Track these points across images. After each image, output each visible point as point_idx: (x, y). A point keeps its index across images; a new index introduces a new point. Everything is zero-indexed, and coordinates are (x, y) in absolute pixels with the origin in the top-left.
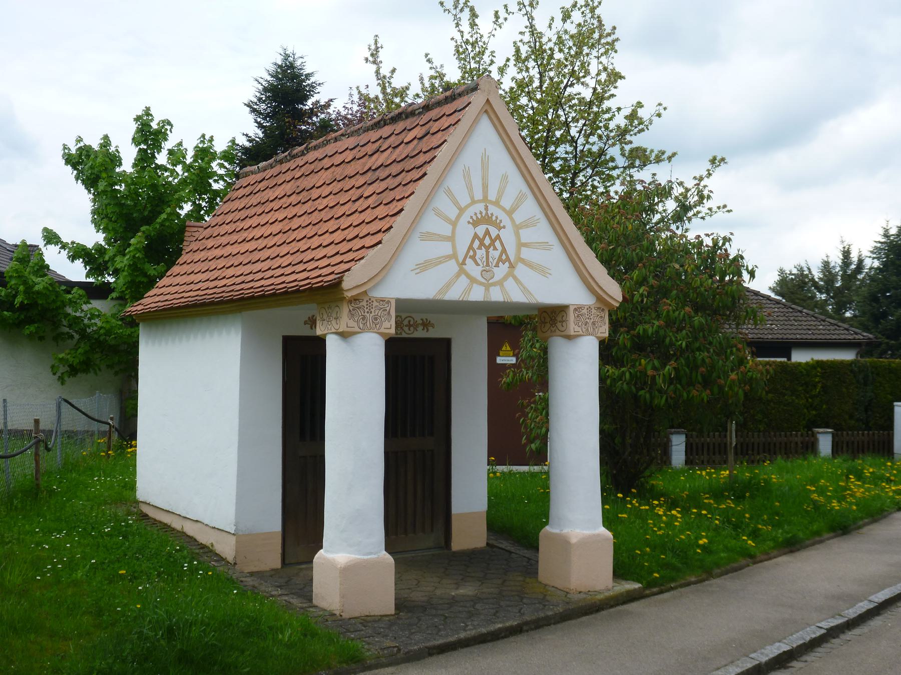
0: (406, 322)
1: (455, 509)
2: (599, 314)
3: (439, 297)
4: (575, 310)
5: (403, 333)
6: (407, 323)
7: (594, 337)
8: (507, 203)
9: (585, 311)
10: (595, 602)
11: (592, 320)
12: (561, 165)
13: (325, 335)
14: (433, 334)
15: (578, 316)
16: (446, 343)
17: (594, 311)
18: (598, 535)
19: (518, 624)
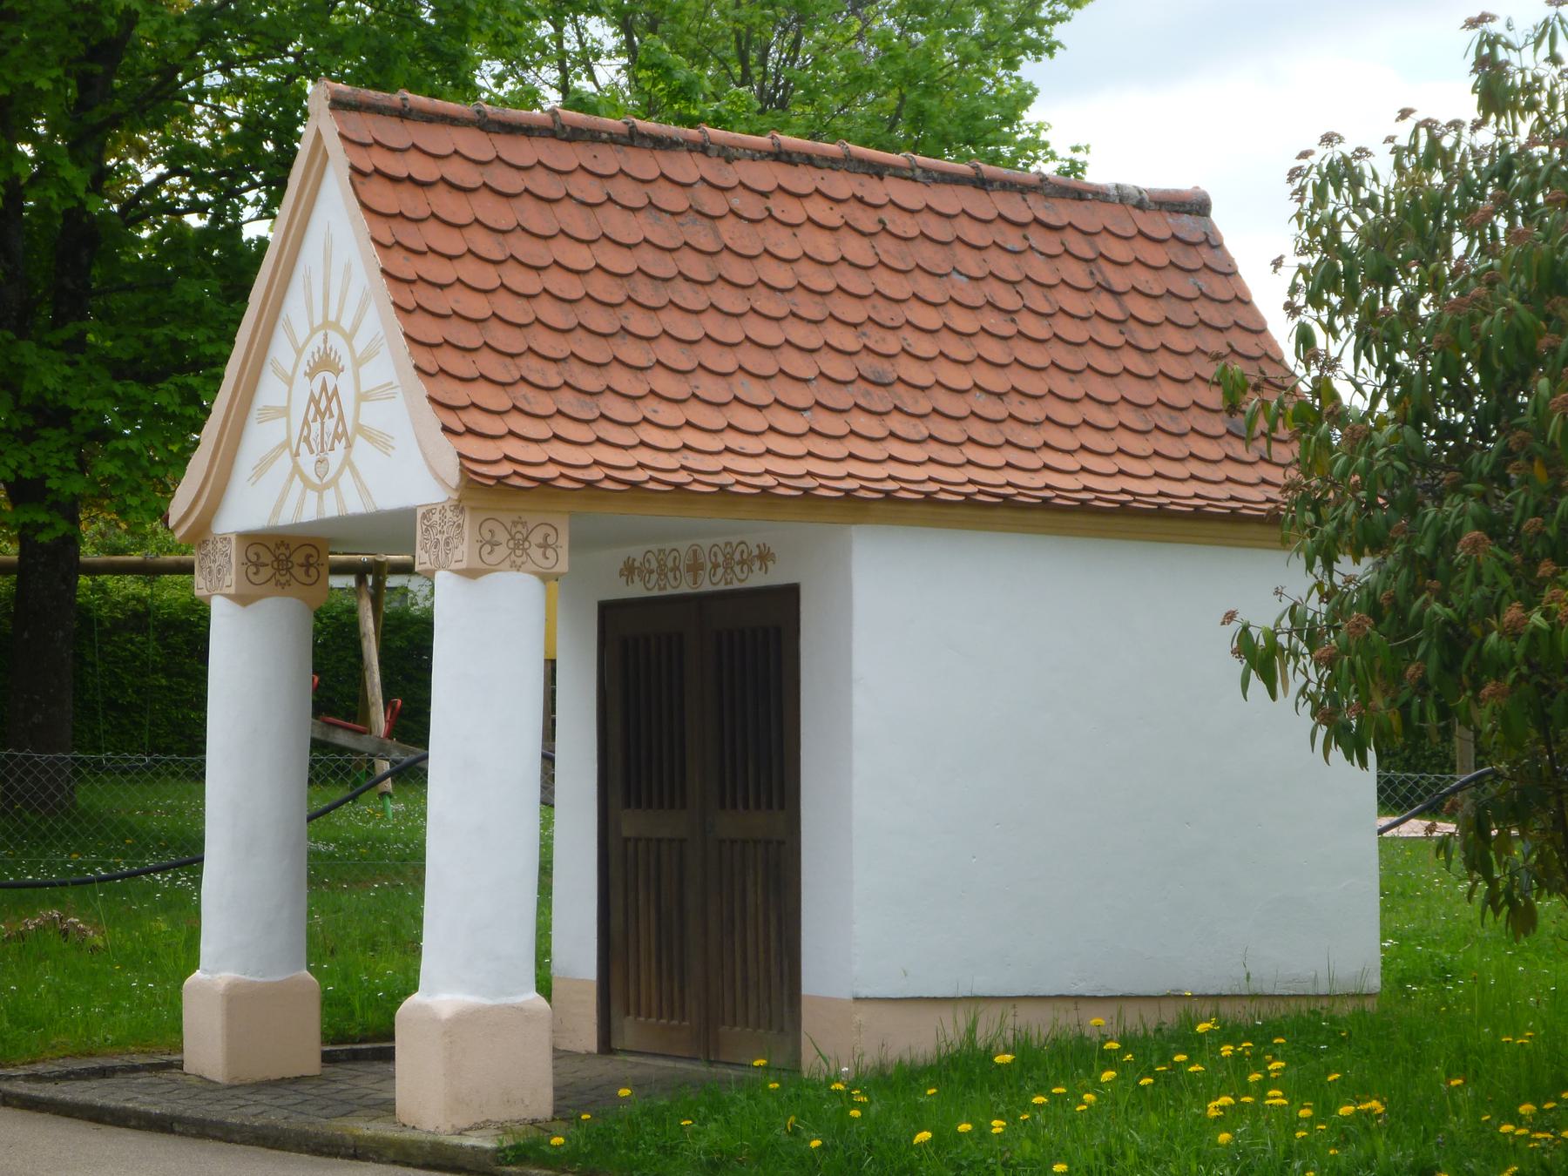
0: (737, 557)
1: (815, 980)
2: (455, 519)
3: (273, 523)
4: (424, 516)
5: (735, 581)
6: (262, 569)
7: (448, 573)
8: (360, 344)
9: (436, 518)
10: (342, 1137)
11: (446, 535)
12: (1012, 152)
13: (209, 598)
14: (757, 579)
15: (427, 530)
16: (790, 594)
17: (449, 514)
18: (518, 1009)
19: (161, 1114)
